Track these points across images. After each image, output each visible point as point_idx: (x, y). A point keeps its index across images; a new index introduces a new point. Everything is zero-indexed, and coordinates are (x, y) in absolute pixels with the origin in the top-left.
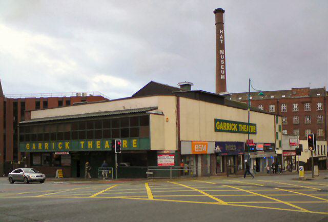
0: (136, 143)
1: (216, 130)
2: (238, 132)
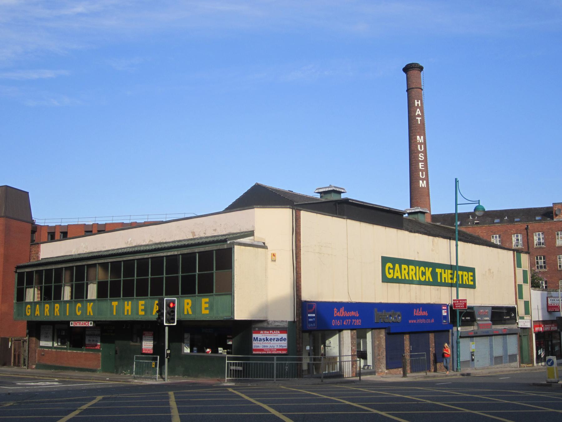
0: (207, 306)
1: (385, 280)
2: (435, 282)
